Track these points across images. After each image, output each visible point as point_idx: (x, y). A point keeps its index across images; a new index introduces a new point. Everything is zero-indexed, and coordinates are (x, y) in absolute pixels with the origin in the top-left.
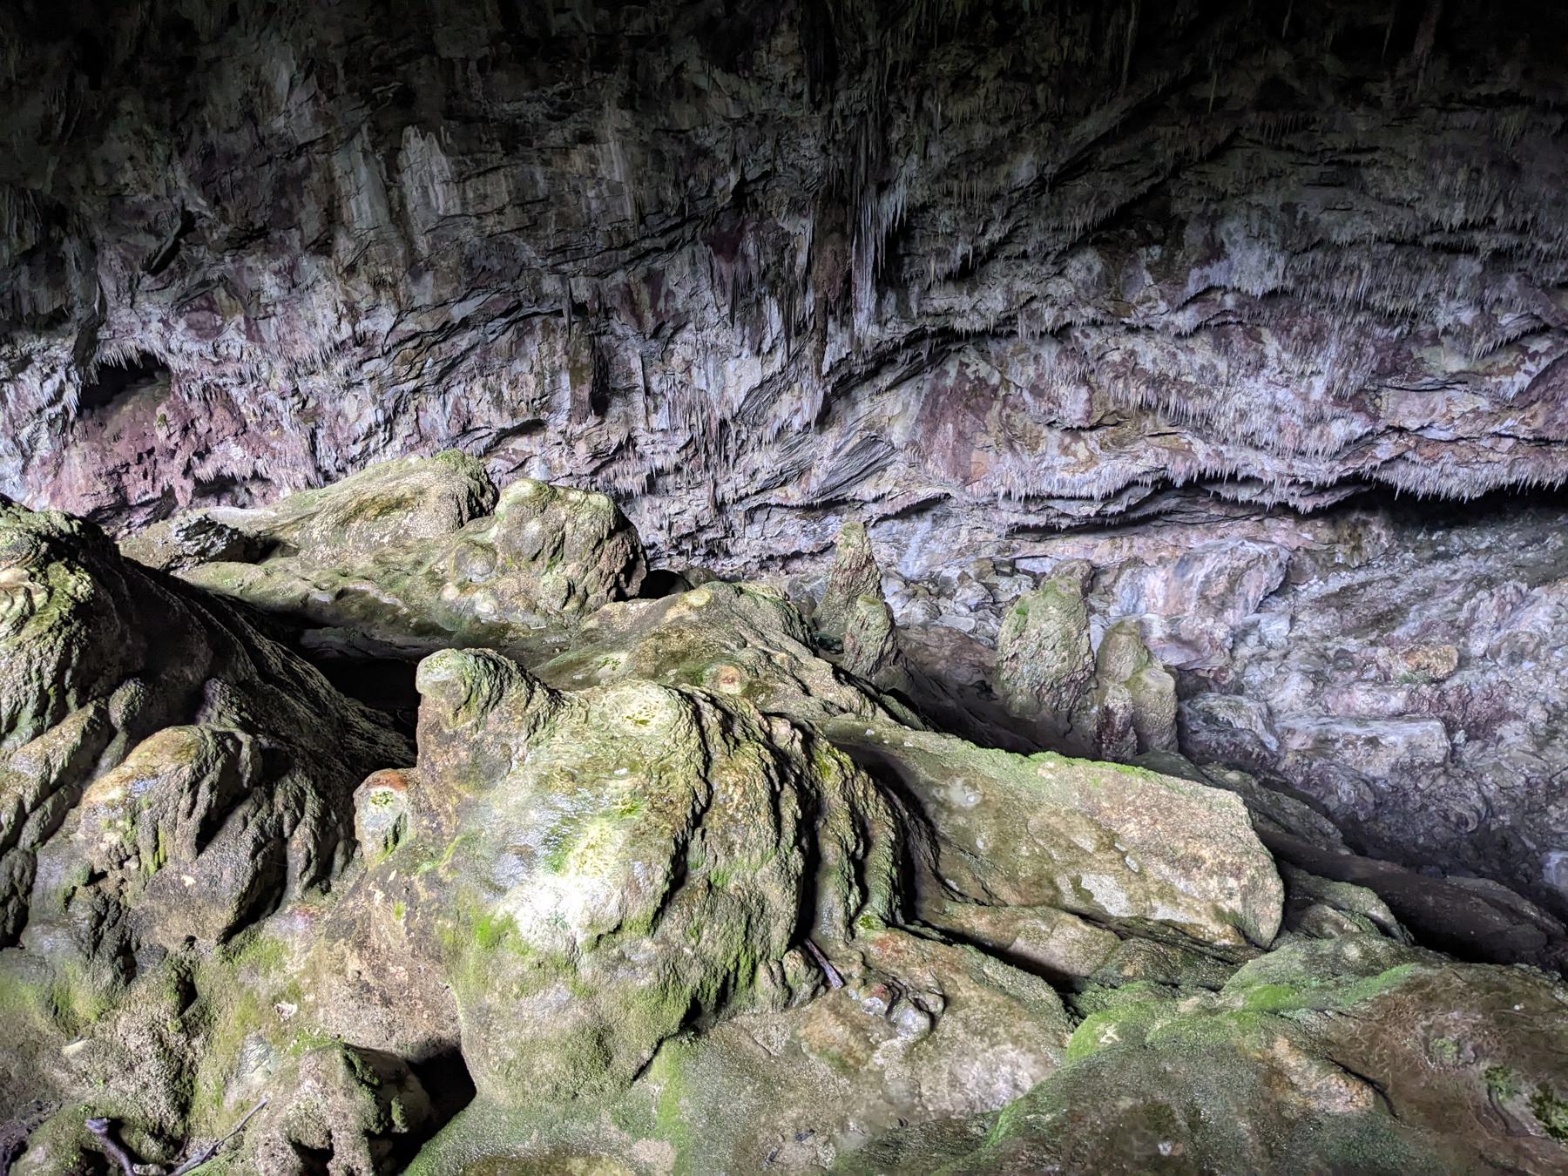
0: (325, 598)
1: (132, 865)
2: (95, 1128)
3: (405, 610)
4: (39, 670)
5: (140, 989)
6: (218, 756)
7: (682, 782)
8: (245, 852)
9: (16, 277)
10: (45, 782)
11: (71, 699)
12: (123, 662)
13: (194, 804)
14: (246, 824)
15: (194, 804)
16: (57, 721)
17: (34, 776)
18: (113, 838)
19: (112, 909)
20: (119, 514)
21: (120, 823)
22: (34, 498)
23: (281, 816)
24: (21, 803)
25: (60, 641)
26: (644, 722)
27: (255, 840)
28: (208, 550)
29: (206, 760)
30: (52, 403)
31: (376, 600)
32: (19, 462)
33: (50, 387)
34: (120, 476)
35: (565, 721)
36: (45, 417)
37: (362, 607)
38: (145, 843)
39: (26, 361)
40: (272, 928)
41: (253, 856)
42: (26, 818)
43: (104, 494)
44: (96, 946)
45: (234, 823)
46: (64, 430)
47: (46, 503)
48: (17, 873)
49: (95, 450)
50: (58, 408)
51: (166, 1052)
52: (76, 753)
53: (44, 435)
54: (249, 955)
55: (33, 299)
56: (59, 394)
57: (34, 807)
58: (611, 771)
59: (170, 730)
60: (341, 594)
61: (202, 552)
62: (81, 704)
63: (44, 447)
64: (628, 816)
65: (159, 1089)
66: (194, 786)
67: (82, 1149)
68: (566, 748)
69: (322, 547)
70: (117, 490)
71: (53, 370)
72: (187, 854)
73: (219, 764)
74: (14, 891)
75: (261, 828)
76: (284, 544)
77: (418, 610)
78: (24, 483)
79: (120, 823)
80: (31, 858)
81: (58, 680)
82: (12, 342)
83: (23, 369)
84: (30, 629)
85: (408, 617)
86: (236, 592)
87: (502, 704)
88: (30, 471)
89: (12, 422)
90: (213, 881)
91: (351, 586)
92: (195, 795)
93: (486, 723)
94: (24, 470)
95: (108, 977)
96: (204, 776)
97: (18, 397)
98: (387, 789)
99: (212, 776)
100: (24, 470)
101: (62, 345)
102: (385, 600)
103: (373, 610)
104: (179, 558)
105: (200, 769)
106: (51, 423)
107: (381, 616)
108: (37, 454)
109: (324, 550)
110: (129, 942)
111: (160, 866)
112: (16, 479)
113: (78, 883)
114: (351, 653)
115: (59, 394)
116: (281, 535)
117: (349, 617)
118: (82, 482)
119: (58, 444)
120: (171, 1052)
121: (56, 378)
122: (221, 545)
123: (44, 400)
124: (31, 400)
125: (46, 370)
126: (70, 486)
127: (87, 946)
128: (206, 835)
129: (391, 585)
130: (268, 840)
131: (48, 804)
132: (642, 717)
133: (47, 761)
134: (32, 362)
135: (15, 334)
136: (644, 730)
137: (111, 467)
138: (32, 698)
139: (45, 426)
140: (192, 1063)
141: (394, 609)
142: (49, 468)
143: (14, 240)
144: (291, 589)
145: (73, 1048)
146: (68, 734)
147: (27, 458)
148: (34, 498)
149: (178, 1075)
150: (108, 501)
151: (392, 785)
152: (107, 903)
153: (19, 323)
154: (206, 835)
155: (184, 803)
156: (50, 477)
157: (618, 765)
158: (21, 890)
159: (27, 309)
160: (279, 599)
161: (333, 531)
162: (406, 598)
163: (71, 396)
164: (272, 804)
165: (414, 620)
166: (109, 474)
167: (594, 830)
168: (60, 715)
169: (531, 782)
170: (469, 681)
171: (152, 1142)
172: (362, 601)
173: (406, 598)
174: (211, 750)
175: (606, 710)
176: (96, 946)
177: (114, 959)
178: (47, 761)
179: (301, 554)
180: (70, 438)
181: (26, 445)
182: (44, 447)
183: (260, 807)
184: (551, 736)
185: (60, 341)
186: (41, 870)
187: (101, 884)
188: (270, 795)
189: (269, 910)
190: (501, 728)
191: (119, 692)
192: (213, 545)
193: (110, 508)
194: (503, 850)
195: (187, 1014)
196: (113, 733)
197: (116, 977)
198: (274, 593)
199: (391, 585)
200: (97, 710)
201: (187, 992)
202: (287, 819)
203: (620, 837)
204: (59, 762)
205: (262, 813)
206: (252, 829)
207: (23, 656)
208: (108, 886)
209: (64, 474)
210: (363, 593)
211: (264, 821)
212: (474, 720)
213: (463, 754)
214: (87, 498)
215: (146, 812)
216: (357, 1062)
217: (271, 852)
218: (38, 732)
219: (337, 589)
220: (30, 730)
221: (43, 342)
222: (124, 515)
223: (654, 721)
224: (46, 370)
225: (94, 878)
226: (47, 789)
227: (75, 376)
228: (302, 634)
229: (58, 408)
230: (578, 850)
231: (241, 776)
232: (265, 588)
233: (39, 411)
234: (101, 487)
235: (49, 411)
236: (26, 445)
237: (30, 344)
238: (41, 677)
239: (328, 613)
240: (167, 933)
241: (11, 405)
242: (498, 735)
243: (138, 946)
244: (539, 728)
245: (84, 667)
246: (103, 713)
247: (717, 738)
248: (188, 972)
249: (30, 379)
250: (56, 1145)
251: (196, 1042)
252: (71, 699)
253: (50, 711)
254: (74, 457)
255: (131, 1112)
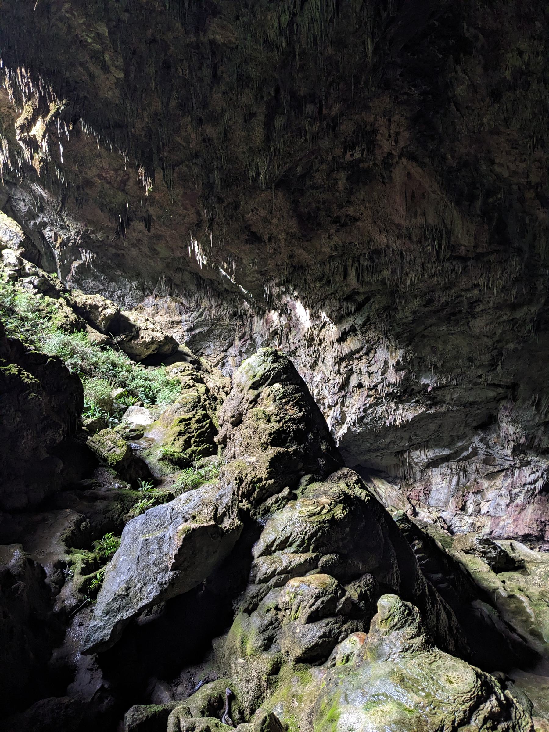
0: (504, 594)
1: (288, 612)
2: (228, 692)
3: (533, 620)
4: (306, 532)
5: (265, 655)
6: (332, 593)
7: (440, 718)
8: (320, 632)
9: (538, 430)
10: (286, 569)
11: (311, 548)
12: (338, 547)
13: (313, 604)
14: (327, 625)
15: (313, 604)
16: (303, 552)
17: (285, 564)
18: (287, 598)
19: (277, 623)
20: (538, 541)
21: (291, 595)
22: (507, 518)
23: (341, 632)
24: (275, 570)
25: (317, 527)
26: (451, 682)
27: (325, 632)
28: (488, 553)
29: (326, 592)
30: (531, 484)
31: (524, 608)
32: (508, 501)
33: (533, 477)
34: (545, 525)
35: (423, 657)
36: (526, 488)
37: (516, 607)
38: (295, 607)
39: (528, 463)
40: (314, 671)
41: (320, 638)
42: (275, 576)
43: (535, 529)
44: (264, 631)
45: (324, 622)
46: (531, 496)
47: (510, 522)
48: (261, 591)
49: (540, 510)
50: (533, 487)
51: (259, 686)
52: (300, 565)
53: (522, 495)
54: (300, 674)
55: (540, 440)
56: (535, 481)
57: (279, 574)
58: (419, 690)
59: (326, 575)
60: (512, 597)
61: (484, 553)
62: (313, 552)
63: (520, 500)
64: (406, 712)
65: (250, 696)
66: (317, 598)
67: (220, 695)
68: (412, 668)
69: (537, 578)
70: (541, 530)
71: (537, 471)
72: (303, 621)
73: (330, 596)
74: (257, 596)
75: (331, 630)
76: (526, 569)
77: (539, 623)
78: (506, 510)
79: (291, 595)
80: (269, 589)
81: (310, 539)
82: (526, 454)
83: (526, 466)
84: (313, 518)
85: (532, 623)
86: (471, 571)
87: (401, 631)
88: (510, 507)
89: (512, 484)
90: (304, 636)
91: (518, 596)
92: (316, 601)
93: (390, 634)
94: (508, 505)
95: (259, 644)
96: (322, 597)
97: (519, 476)
98: (357, 639)
99: (325, 599)
100: (508, 505)
101: (545, 462)
102: (528, 610)
103: (520, 611)
104: (474, 550)
105: (322, 593)
106: (527, 491)
107: (521, 616)
108: (516, 501)
109: (537, 580)
110: (273, 638)
111: (295, 619)
112: (504, 507)
113: (273, 606)
114: (486, 619)
115: (535, 481)
116: (528, 565)
117: (507, 608)
118: (528, 520)
119: (526, 501)
120: (261, 687)
121: (537, 474)
122: (494, 554)
123: (528, 481)
124: (523, 479)
125: (534, 470)
126: (523, 520)
127: (261, 629)
128: (312, 619)
129: (536, 605)
130: (330, 636)
131: (283, 576)
132: (453, 680)
133: (291, 562)
134: (530, 464)
135: (528, 452)
136: (448, 685)
137: (543, 519)
138: (300, 540)
139: (524, 491)
140: (264, 698)
141: (529, 616)
142: (518, 509)
143: (543, 416)
144: (494, 583)
145: (241, 661)
146: (301, 558)
147: (511, 501)
148: (507, 518)
149: (258, 698)
150: (535, 533)
151: (360, 640)
152: (276, 620)
153: (531, 448)
154: (312, 619)
155: (312, 601)
156: (517, 513)
157: (423, 690)
158: (259, 597)
159: (536, 443)
160: (485, 584)
161: (545, 573)
162: (538, 615)
163: (540, 484)
164: (342, 625)
165: (533, 626)
166: (541, 522)
167: (389, 707)
168: (306, 551)
169: (388, 669)
170: (392, 612)
171: (237, 713)
172: (517, 604)
173: (538, 615)
174: (331, 589)
175: (443, 666)
176: (264, 631)
177: (265, 640)
178: (291, 562)
179: (529, 577)
180: (532, 501)
181: (513, 496)
182: (520, 500)
183: (336, 623)
184: (411, 658)
185: (545, 460)
186: (268, 595)
187: (279, 612)
188: (344, 622)
189: (317, 663)
190: (394, 640)
191: (328, 556)
192: (490, 552)
193: (535, 536)
194: (360, 688)
195: (271, 677)
196: (317, 567)
197: (261, 646)
198: (486, 580)
199: (536, 605)
200: (316, 556)
201: (276, 669)
202: (343, 634)
203: (395, 716)
204: (294, 564)
205: (336, 626)
206: (328, 628)
207: (305, 525)
208: (280, 614)
209: (523, 514)
210: (522, 602)
211: (333, 629)
212: (386, 629)
213: (376, 640)
214: (527, 528)
215: (300, 596)
216: (267, 722)
217: (329, 642)
218: (296, 552)
219: (511, 593)
220: (294, 550)
221: (538, 458)
222: (540, 542)
223: (455, 685)
224: (534, 470)
225: (277, 609)
226: (285, 571)
227: (545, 477)
228: (475, 599)
229: (533, 487)
230: (378, 709)
231: (336, 607)
232: (484, 576)
233: (525, 485)
234: (535, 526)
235: (528, 486)
236: (513, 496)
237: (532, 457)
238: (305, 535)
239: (500, 601)
240: (284, 643)
241: (515, 478)
242: (391, 642)
243: (275, 642)
244: (409, 652)
245: (321, 540)
246: (317, 559)
247: (481, 717)
248: (281, 663)
249: (527, 471)
250: (216, 687)
251: (269, 691)
252: (311, 548)
253: (303, 548)
254: (530, 509)
255: (239, 697)
